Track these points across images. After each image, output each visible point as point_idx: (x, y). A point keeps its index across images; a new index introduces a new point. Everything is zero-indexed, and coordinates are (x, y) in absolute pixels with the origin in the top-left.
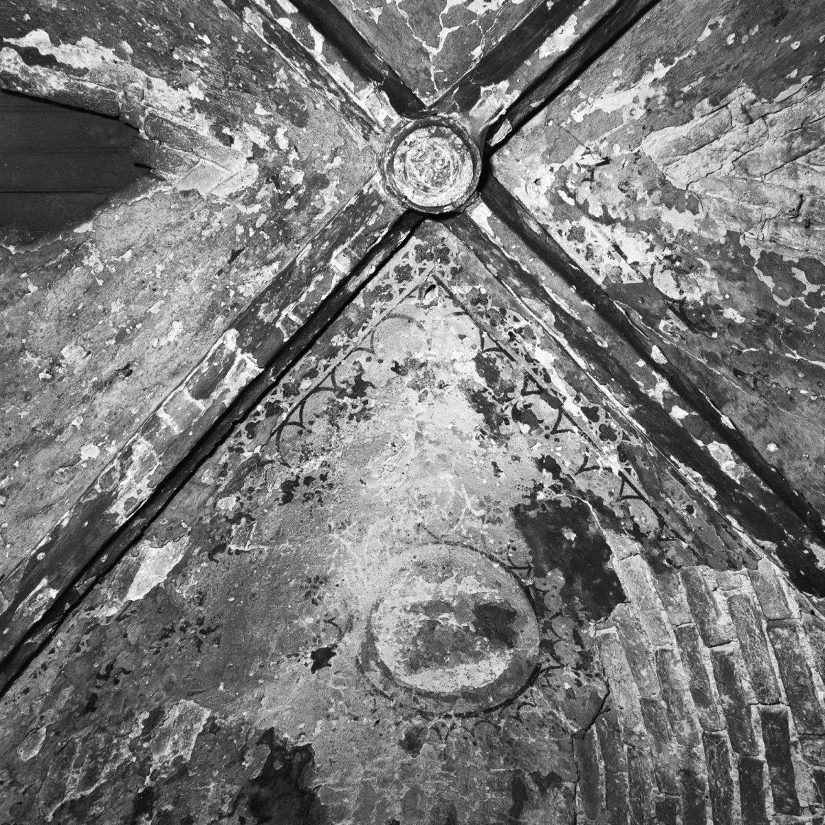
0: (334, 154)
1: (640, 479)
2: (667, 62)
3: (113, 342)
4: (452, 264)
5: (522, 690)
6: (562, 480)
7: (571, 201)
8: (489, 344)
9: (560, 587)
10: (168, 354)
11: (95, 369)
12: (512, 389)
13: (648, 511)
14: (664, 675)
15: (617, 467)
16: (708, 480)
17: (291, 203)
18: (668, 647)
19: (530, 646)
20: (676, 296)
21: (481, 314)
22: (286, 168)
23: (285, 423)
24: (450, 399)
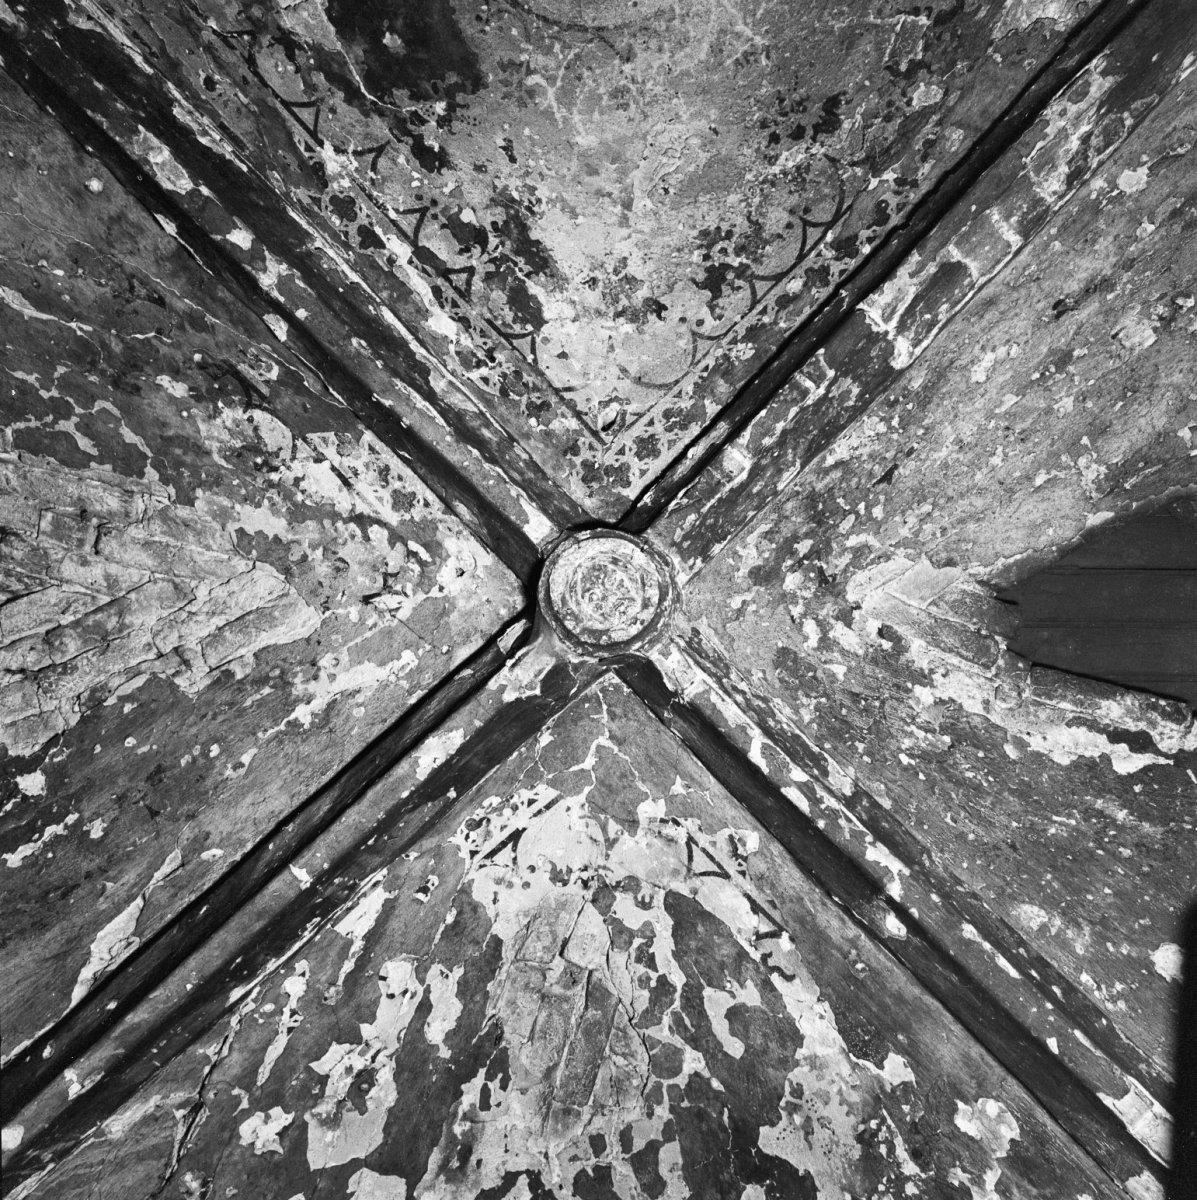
0: (740, 612)
1: (290, 135)
2: (295, 725)
3: (1076, 353)
4: (578, 460)
6: (409, 133)
7: (413, 546)
8: (524, 344)
10: (997, 334)
13: (275, 82)
15: (327, 153)
17: (803, 547)
21: (536, 388)
22: (808, 594)
23: (829, 226)
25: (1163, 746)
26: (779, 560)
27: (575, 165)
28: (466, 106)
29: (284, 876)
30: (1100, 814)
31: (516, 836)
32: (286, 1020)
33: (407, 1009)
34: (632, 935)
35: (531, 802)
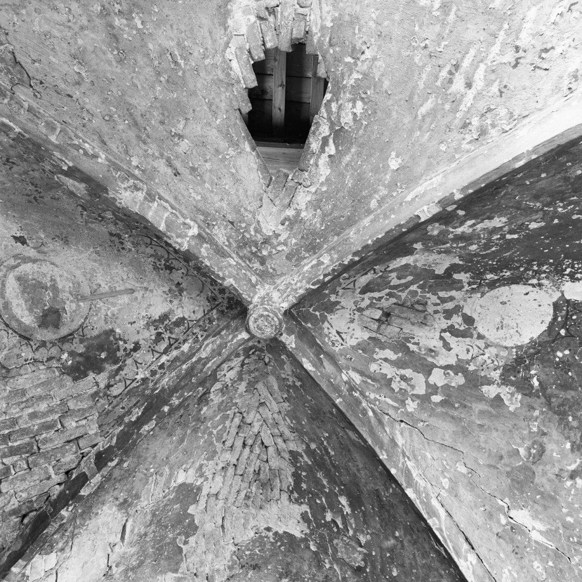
0: (274, 270)
1: (135, 387)
2: (301, 386)
3: (191, 165)
4: (226, 311)
5: (15, 332)
6: (130, 353)
7: (251, 353)
8: (191, 324)
9: (76, 350)
10: (185, 193)
11: (177, 157)
12: (171, 332)
13: (120, 391)
14: (40, 398)
15: (139, 377)
16: (138, 418)
17: (254, 249)
18: (54, 400)
19: (41, 335)
20: (212, 391)
21: (204, 321)
22: (269, 248)
23: (151, 239)
24: (165, 304)
25: (328, 134)
26: (258, 256)
27: (135, 304)
28: (120, 335)
29: (338, 405)
30: (347, 165)
31: (338, 333)
32: (383, 398)
33: (385, 364)
34: (372, 302)
35: (328, 329)
